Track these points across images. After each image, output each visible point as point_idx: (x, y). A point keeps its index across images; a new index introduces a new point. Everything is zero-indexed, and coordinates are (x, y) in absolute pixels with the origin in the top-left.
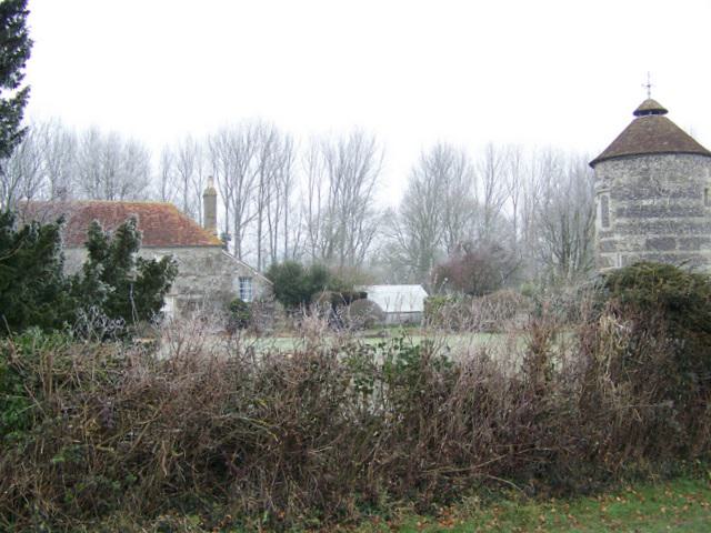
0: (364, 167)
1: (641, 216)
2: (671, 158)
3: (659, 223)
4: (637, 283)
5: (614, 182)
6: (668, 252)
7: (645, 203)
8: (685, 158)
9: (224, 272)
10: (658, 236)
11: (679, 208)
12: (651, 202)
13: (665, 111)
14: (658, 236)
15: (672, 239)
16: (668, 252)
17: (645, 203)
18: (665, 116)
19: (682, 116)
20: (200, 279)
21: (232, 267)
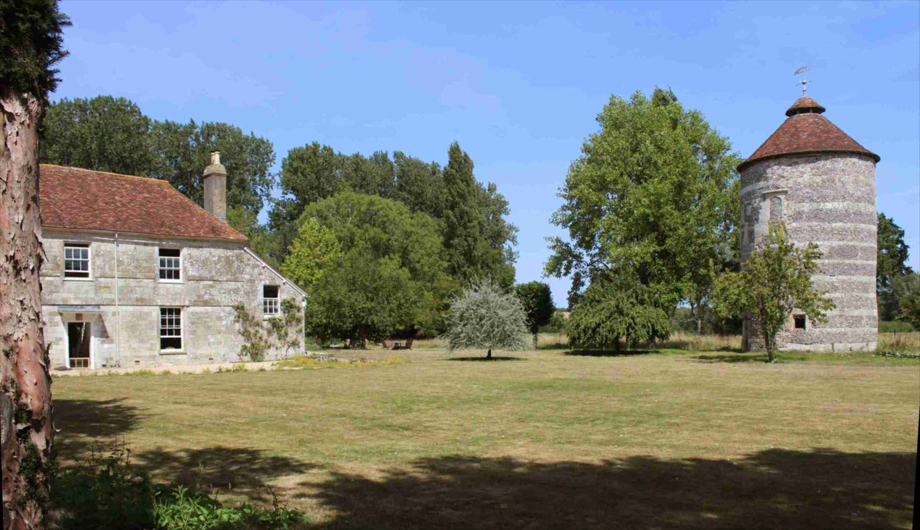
0: (718, 350)
1: (823, 220)
2: (855, 160)
3: (844, 229)
4: (661, 240)
5: (791, 181)
6: (851, 261)
7: (829, 206)
8: (826, 164)
9: (247, 277)
10: (841, 243)
11: (861, 214)
12: (836, 204)
13: (819, 110)
14: (841, 243)
15: (854, 247)
16: (851, 261)
17: (829, 206)
18: (823, 114)
19: (842, 117)
20: (218, 286)
21: (256, 271)
